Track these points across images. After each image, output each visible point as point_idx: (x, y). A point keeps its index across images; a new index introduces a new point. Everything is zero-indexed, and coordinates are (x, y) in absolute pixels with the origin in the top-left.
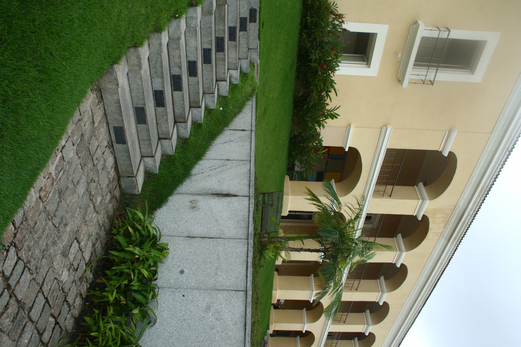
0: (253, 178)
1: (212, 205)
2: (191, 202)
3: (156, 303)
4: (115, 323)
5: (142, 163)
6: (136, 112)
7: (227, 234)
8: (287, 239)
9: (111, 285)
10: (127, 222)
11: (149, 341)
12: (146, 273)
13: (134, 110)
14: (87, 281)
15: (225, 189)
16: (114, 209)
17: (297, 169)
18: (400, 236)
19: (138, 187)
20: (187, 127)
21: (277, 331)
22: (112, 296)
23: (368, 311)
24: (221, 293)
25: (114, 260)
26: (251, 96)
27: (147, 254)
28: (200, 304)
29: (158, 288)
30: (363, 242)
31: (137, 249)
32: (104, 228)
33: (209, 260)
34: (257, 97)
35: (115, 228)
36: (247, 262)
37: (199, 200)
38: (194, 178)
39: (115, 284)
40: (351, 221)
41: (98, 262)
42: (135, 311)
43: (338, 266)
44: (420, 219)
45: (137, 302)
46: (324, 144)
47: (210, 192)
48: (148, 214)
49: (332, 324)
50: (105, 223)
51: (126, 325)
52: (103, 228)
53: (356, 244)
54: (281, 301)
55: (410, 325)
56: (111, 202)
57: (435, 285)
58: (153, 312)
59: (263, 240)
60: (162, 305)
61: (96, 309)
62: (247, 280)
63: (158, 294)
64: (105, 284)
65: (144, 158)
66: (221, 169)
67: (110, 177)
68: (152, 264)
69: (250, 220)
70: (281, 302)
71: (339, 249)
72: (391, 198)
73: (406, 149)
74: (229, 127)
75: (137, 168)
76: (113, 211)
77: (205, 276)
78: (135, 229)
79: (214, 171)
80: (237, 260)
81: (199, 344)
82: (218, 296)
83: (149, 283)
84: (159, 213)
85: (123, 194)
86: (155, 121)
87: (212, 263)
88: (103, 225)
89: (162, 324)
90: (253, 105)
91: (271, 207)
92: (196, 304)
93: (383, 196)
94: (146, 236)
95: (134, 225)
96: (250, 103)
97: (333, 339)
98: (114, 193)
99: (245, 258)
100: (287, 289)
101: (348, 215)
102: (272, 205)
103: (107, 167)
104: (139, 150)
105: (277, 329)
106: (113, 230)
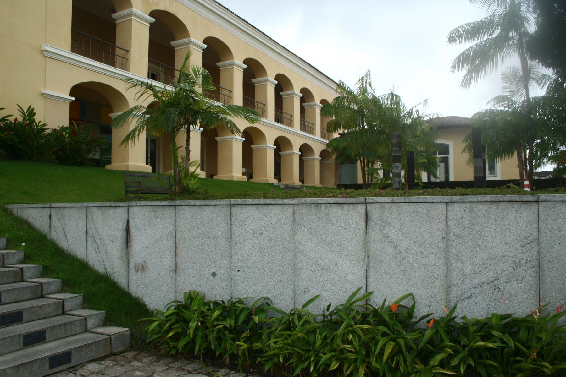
0: (108, 204)
1: (140, 247)
2: (137, 271)
3: (247, 299)
4: (269, 339)
5: (94, 330)
6: (30, 345)
7: (171, 229)
8: (176, 165)
9: (230, 349)
10: (163, 339)
11: (286, 302)
12: (217, 313)
13: (26, 347)
14: (229, 374)
15: (120, 234)
16: (149, 356)
17: (97, 156)
18: (173, 43)
19: (122, 332)
20: (48, 283)
21: (275, 175)
22: (243, 346)
23: (253, 80)
24: (234, 231)
25: (205, 348)
26: (6, 210)
27: (197, 313)
28: (247, 254)
29: (232, 298)
30: (179, 81)
31: (191, 324)
32: (170, 364)
33: (200, 247)
34: (8, 204)
35: (170, 351)
36: (200, 205)
37: (134, 262)
38: (109, 270)
39: (230, 344)
40: (155, 94)
41: (207, 366)
42: (256, 320)
43: (204, 110)
44: (154, 20)
45: (247, 320)
46: (66, 124)
47: (125, 251)
48: (153, 317)
49: (266, 118)
50: (165, 363)
51: (271, 328)
52: (171, 365)
53: (180, 89)
54: (244, 172)
55: (267, 37)
56: (141, 359)
57: (226, 8)
58: (257, 301)
59: (178, 191)
60: (249, 292)
61: (257, 361)
62: (219, 205)
63: (238, 298)
64: (230, 355)
65: (88, 329)
66: (98, 240)
67: (111, 365)
68: (207, 307)
69: (154, 205)
70: (245, 171)
71: (185, 108)
72: (130, 51)
73: (72, 29)
74: (47, 235)
75: (100, 335)
76: (152, 356)
77: (217, 250)
78: (170, 329)
79: (100, 247)
80: (199, 216)
81: (286, 251)
82: (237, 234)
83: (227, 309)
84: (151, 305)
85: (131, 348)
86: (41, 321)
87: (203, 243)
88: (167, 365)
89: (269, 291)
90: (17, 207)
91: (141, 184)
92: (246, 257)
93: (128, 59)
94: (177, 317)
95: (165, 331)
96: (15, 211)
97: (281, 117)
98: (130, 358)
99: (196, 208)
100: (231, 165)
101: (148, 99)
102: (140, 183)
103: (100, 369)
104: (78, 335)
105: (273, 175)
106: (172, 354)
